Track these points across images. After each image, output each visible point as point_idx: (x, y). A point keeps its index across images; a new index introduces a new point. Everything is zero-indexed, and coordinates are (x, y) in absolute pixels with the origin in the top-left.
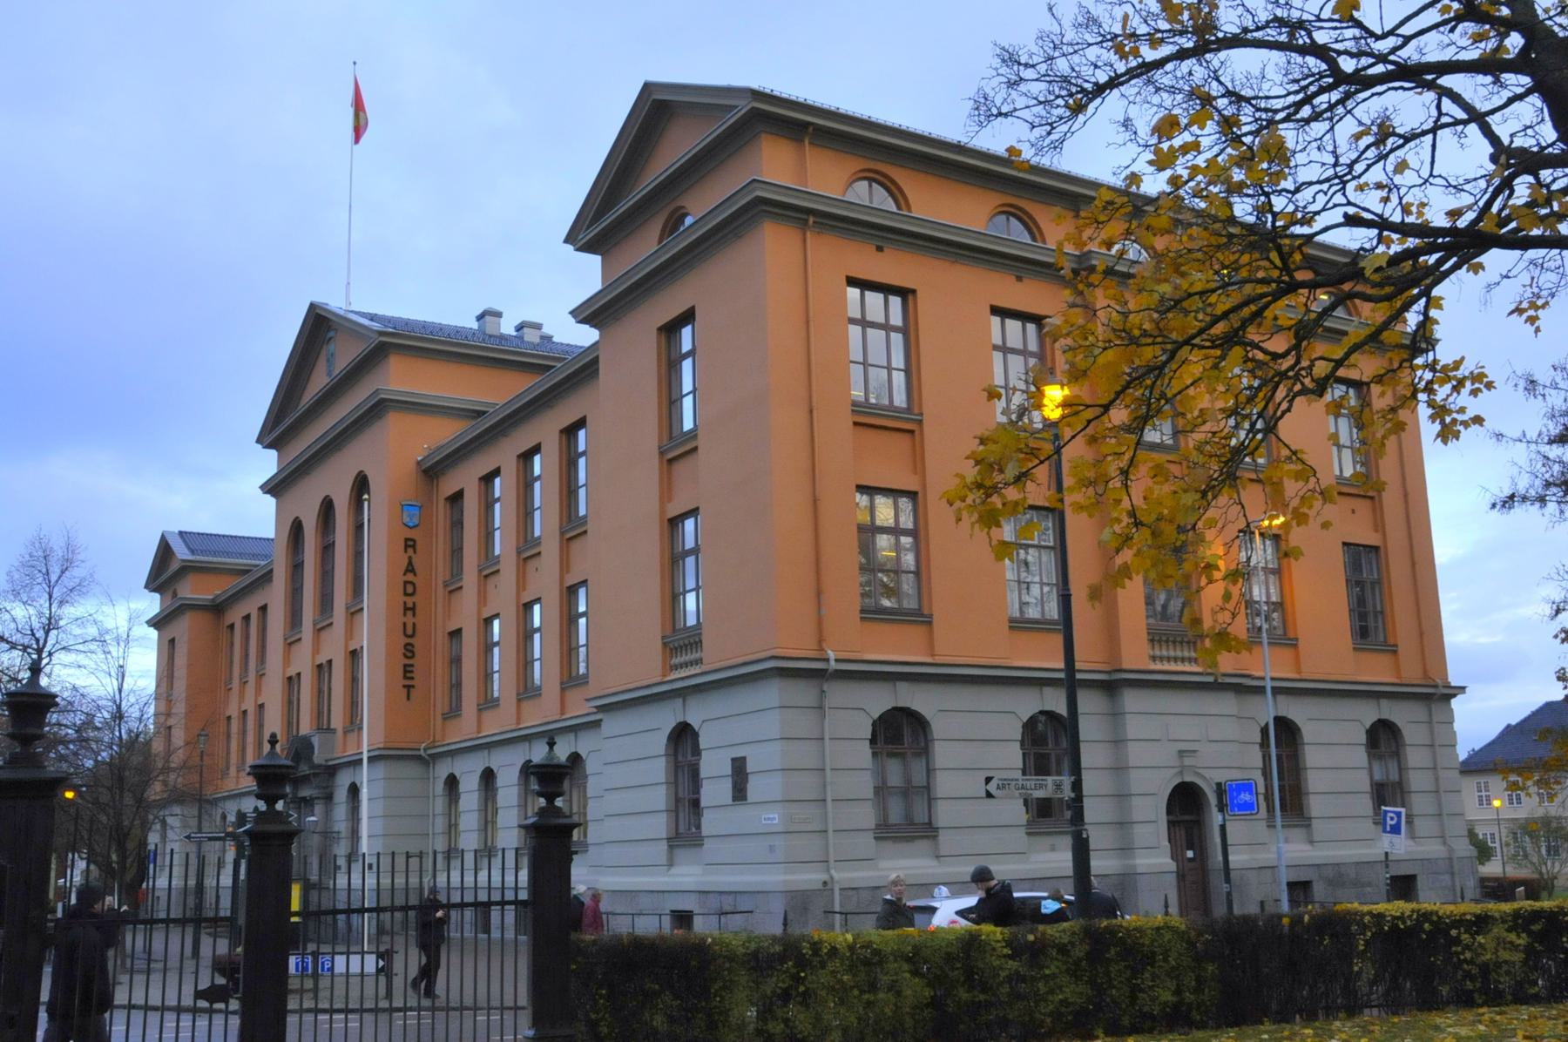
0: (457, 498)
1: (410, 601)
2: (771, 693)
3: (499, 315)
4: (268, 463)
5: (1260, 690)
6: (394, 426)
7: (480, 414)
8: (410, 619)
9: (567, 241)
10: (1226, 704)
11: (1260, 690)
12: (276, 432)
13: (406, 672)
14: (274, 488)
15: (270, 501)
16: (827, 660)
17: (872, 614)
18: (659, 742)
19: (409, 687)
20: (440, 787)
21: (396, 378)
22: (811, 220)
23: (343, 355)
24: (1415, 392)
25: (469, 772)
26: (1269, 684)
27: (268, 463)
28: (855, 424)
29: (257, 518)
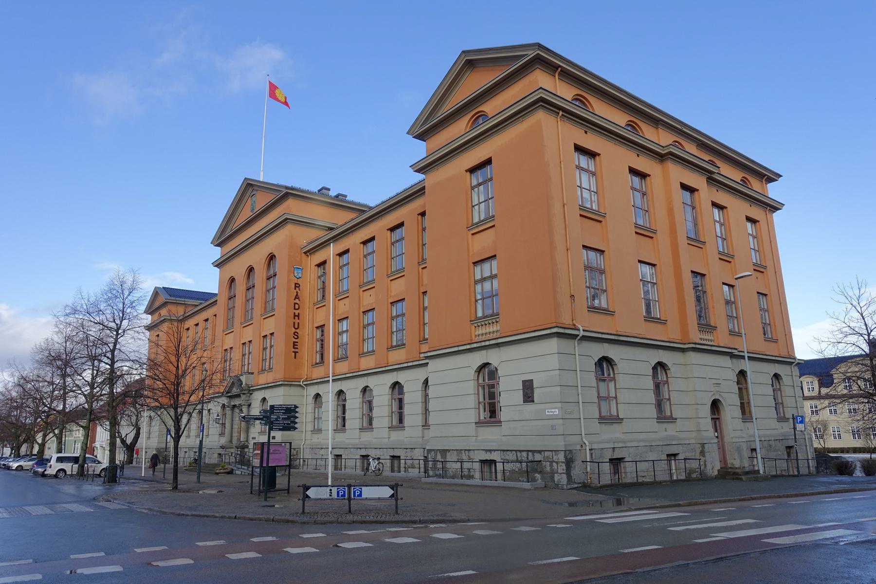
0: (322, 264)
1: (297, 312)
2: (553, 344)
3: (329, 190)
4: (217, 253)
5: (743, 357)
6: (288, 230)
7: (331, 229)
8: (297, 321)
9: (408, 133)
10: (726, 361)
11: (743, 357)
12: (220, 241)
13: (294, 345)
14: (219, 264)
15: (217, 270)
16: (579, 330)
17: (592, 309)
18: (471, 373)
19: (295, 353)
20: (310, 400)
21: (291, 207)
22: (561, 113)
23: (262, 200)
24: (483, 299)
25: (353, 389)
26: (746, 355)
27: (217, 253)
28: (581, 215)
29: (207, 280)
